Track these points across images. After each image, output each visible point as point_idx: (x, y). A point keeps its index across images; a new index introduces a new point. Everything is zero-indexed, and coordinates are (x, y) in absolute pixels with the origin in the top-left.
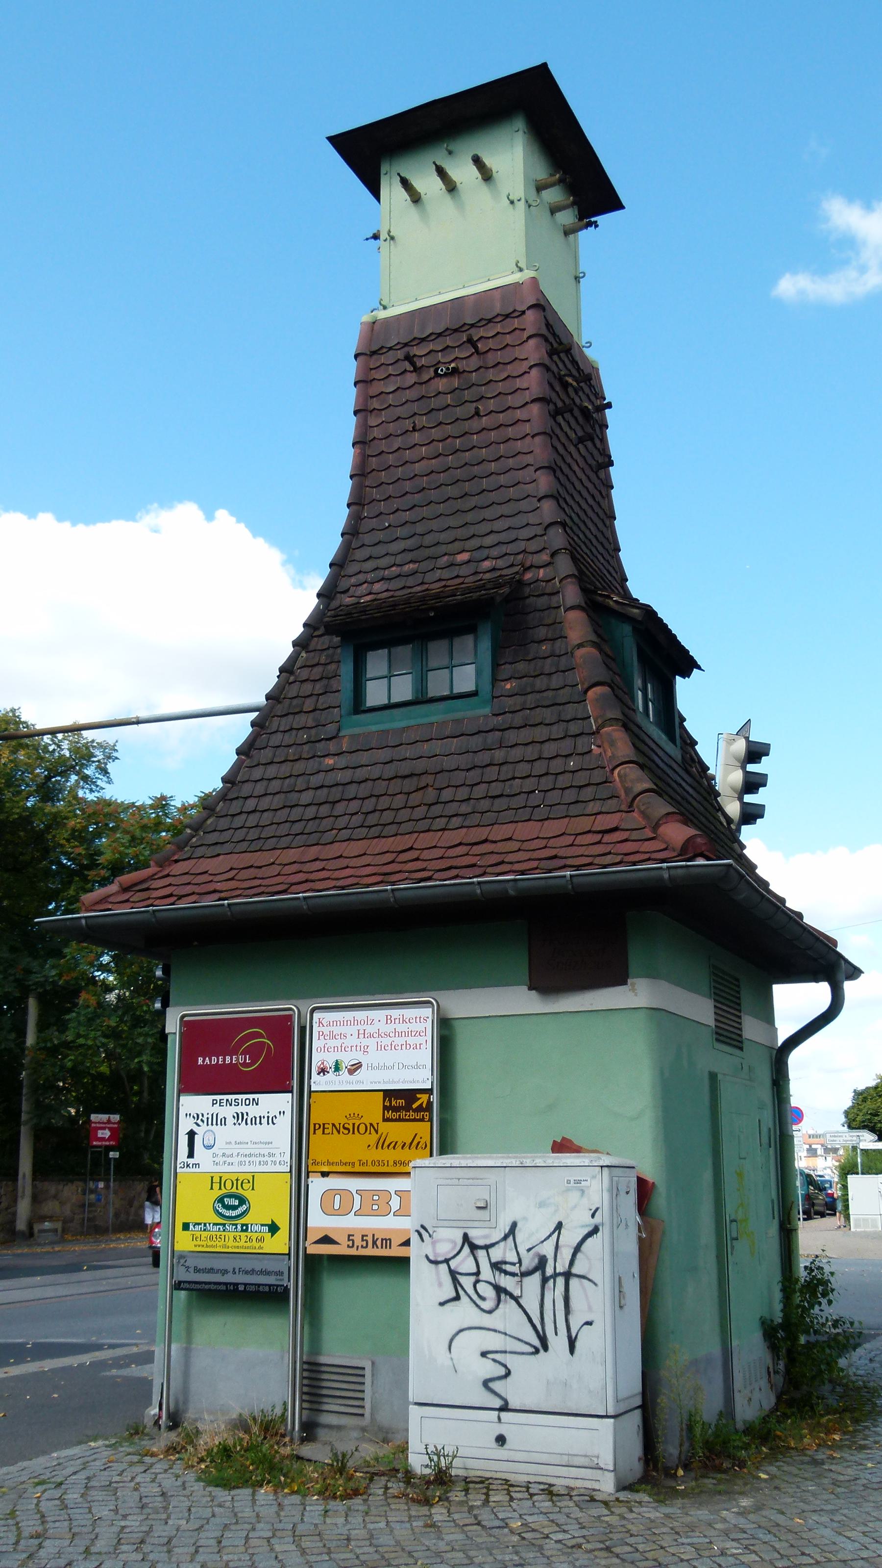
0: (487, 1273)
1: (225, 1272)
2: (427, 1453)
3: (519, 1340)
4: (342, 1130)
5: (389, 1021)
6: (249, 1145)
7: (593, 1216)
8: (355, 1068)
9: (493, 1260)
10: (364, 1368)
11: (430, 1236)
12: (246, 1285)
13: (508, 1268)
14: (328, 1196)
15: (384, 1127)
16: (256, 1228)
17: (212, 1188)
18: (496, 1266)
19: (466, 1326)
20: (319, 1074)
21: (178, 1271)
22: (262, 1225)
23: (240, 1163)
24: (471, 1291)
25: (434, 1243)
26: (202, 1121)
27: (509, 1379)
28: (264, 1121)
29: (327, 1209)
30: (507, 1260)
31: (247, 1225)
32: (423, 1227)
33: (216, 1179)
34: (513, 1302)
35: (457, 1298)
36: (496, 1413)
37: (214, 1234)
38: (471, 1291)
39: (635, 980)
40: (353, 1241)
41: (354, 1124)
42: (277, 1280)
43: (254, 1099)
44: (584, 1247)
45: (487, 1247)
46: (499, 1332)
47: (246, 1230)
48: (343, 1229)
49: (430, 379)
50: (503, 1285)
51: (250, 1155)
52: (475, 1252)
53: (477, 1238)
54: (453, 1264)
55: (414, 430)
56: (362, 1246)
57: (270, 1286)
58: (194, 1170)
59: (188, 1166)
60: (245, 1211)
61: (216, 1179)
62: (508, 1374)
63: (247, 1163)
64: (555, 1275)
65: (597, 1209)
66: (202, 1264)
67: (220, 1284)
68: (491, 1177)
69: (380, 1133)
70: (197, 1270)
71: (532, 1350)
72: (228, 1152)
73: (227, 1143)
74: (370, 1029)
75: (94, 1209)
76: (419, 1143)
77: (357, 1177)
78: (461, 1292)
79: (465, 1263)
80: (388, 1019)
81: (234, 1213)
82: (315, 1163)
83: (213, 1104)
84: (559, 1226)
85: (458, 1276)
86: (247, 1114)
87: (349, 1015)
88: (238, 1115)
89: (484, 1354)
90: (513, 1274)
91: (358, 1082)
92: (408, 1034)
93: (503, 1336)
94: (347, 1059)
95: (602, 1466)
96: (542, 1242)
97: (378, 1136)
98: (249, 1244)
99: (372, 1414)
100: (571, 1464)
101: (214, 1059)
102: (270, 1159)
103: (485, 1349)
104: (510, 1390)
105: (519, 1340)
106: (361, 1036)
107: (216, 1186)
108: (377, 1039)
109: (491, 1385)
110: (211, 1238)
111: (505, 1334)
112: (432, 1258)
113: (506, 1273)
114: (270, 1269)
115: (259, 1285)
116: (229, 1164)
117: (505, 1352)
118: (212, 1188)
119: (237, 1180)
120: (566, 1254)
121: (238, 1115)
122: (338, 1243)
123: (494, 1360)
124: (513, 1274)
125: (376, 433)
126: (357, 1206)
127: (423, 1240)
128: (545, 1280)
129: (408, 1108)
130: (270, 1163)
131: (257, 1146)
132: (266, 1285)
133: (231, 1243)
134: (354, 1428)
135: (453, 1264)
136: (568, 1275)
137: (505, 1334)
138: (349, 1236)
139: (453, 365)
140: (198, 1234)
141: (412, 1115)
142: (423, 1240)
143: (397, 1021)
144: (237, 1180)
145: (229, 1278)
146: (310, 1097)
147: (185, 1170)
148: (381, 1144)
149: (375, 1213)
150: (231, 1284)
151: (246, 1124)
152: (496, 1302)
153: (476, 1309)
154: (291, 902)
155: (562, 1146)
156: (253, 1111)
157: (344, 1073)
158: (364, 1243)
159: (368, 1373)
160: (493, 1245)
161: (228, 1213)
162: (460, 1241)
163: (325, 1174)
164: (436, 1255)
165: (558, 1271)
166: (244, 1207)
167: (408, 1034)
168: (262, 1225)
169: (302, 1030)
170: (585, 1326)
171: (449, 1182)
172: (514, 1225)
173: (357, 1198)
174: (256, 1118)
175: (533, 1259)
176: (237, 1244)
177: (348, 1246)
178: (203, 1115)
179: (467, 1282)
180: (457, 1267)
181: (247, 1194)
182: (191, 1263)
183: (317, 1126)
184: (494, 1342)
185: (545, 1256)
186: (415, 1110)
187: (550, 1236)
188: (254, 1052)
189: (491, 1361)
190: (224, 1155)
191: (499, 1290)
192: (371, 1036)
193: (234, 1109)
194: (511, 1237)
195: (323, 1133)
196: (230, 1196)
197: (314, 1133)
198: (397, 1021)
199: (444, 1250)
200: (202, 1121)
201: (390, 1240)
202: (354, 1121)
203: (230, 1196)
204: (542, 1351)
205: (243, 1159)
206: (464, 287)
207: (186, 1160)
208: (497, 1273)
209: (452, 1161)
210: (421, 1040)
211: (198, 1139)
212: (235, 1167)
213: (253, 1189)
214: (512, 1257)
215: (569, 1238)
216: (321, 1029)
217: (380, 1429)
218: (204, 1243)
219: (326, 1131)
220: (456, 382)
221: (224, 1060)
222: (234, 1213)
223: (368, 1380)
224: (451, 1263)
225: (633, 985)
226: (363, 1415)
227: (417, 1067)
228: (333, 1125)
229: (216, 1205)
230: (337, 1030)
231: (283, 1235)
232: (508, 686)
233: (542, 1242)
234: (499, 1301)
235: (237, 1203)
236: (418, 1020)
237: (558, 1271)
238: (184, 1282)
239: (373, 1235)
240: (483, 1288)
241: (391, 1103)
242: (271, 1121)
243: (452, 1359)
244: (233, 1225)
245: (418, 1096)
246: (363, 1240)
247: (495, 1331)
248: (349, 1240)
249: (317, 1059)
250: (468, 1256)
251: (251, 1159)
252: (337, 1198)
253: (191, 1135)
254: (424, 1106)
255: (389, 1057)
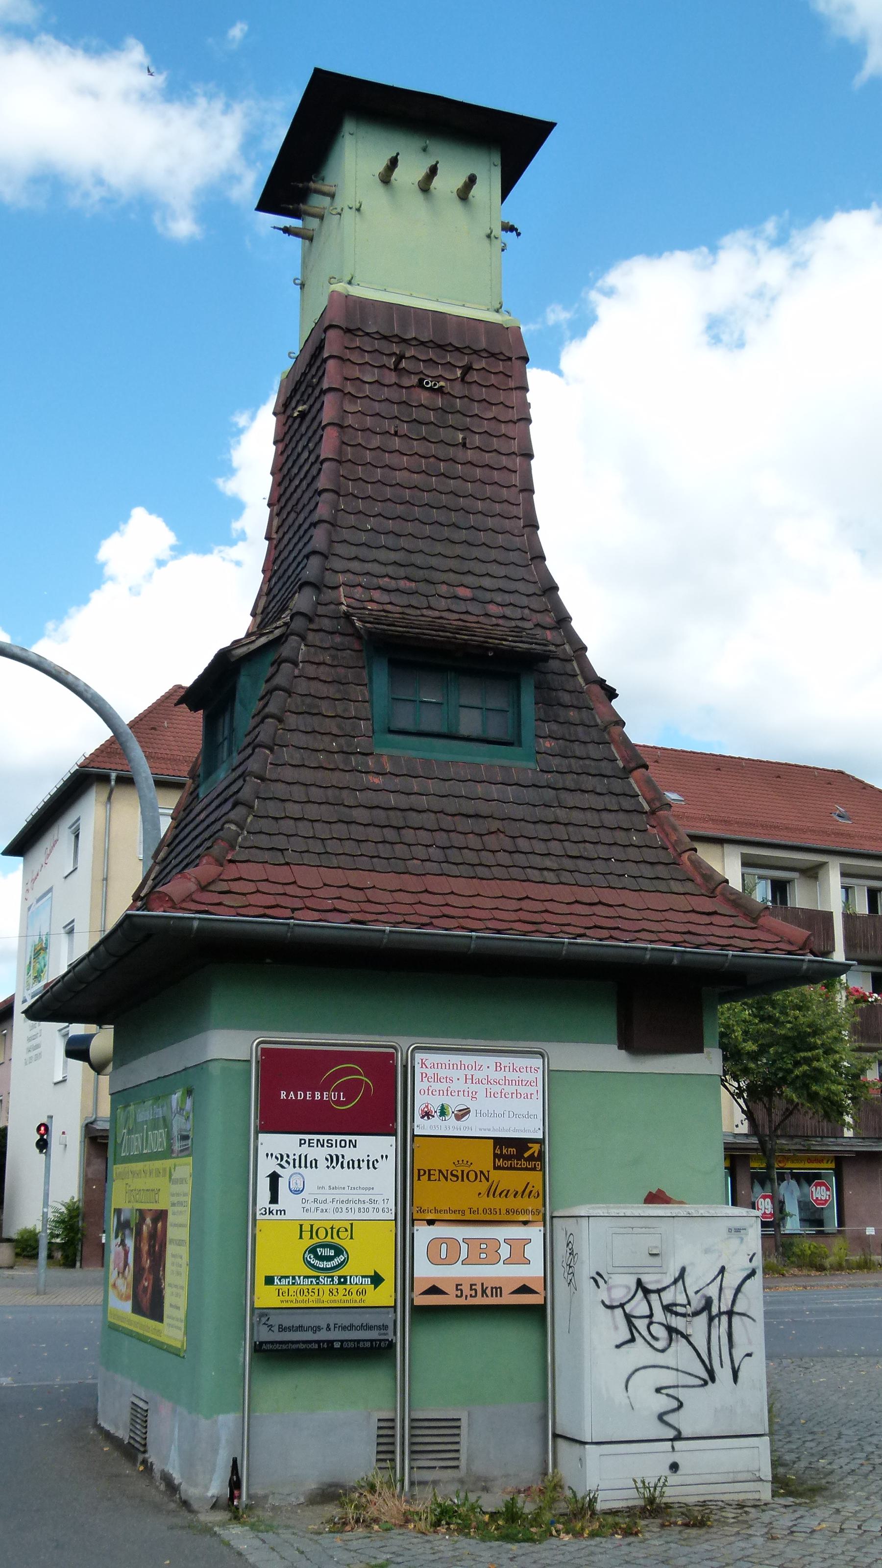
0: (659, 1315)
1: (316, 1329)
2: (637, 1488)
3: (690, 1374)
4: (450, 1176)
5: (499, 1069)
6: (347, 1191)
7: (751, 1260)
8: (462, 1114)
9: (665, 1303)
10: (459, 1420)
11: (606, 1282)
12: (342, 1341)
13: (680, 1309)
14: (434, 1245)
15: (495, 1175)
16: (356, 1280)
17: (301, 1237)
18: (668, 1308)
19: (641, 1365)
20: (423, 1117)
21: (258, 1332)
22: (363, 1277)
23: (336, 1210)
24: (645, 1333)
25: (609, 1289)
26: (288, 1163)
27: (682, 1411)
28: (364, 1165)
29: (434, 1258)
30: (678, 1302)
31: (345, 1277)
32: (598, 1274)
33: (307, 1227)
34: (684, 1341)
35: (633, 1340)
36: (670, 1443)
37: (305, 1287)
38: (645, 1333)
39: (709, 1049)
40: (461, 1290)
41: (463, 1172)
42: (380, 1334)
43: (350, 1141)
44: (744, 1288)
45: (659, 1291)
46: (672, 1369)
47: (345, 1283)
48: (453, 1279)
49: (412, 386)
50: (674, 1325)
51: (348, 1201)
52: (648, 1296)
53: (651, 1282)
54: (628, 1308)
55: (396, 434)
56: (471, 1296)
57: (371, 1341)
58: (279, 1217)
59: (271, 1212)
60: (342, 1262)
61: (307, 1227)
62: (681, 1405)
63: (344, 1210)
64: (720, 1314)
65: (754, 1254)
66: (288, 1321)
67: (310, 1342)
68: (664, 1227)
69: (490, 1181)
70: (282, 1329)
71: (702, 1382)
72: (321, 1198)
73: (319, 1188)
74: (478, 1075)
75: (844, 1264)
76: (531, 1192)
77: (468, 1225)
78: (636, 1334)
79: (639, 1307)
80: (498, 1067)
81: (329, 1265)
82: (421, 1211)
83: (301, 1144)
84: (722, 1270)
85: (633, 1319)
86: (343, 1156)
87: (455, 1058)
88: (331, 1157)
89: (658, 1390)
90: (684, 1315)
91: (466, 1128)
92: (520, 1082)
93: (675, 1372)
94: (454, 1104)
95: (763, 1478)
96: (708, 1285)
97: (489, 1184)
98: (348, 1298)
99: (468, 1465)
100: (736, 1479)
101: (300, 1095)
102: (371, 1206)
103: (659, 1386)
104: (681, 1420)
105: (690, 1374)
106: (469, 1081)
107: (307, 1235)
108: (486, 1086)
109: (666, 1418)
110: (302, 1292)
111: (677, 1370)
112: (607, 1303)
113: (677, 1314)
114: (372, 1323)
115: (359, 1341)
116: (322, 1211)
117: (677, 1386)
118: (301, 1237)
119: (332, 1228)
120: (728, 1295)
121: (331, 1157)
122: (446, 1294)
123: (668, 1395)
124: (684, 1315)
125: (350, 420)
126: (464, 1255)
127: (598, 1287)
128: (711, 1319)
129: (519, 1156)
130: (371, 1210)
131: (355, 1191)
132: (367, 1341)
133: (326, 1297)
134: (453, 1480)
135: (628, 1308)
136: (730, 1313)
137: (677, 1370)
138: (457, 1285)
139: (442, 383)
140: (285, 1288)
141: (524, 1164)
142: (598, 1287)
143: (507, 1069)
144: (332, 1228)
145: (323, 1335)
146: (413, 1141)
147: (267, 1217)
148: (491, 1192)
149: (485, 1261)
150: (324, 1342)
151: (342, 1167)
152: (668, 1341)
153: (650, 1349)
154: (508, 942)
155: (656, 1198)
156: (349, 1154)
157: (451, 1120)
158: (473, 1293)
159: (464, 1424)
160: (664, 1289)
161: (321, 1265)
162: (633, 1287)
163: (431, 1222)
164: (611, 1300)
165: (722, 1310)
166: (342, 1258)
167: (520, 1082)
168: (363, 1277)
169: (405, 1067)
170: (747, 1358)
171: (622, 1231)
172: (683, 1270)
173: (464, 1247)
174: (353, 1161)
175: (700, 1301)
176: (333, 1298)
177: (457, 1296)
178: (288, 1156)
179: (641, 1324)
180: (632, 1310)
181: (345, 1243)
182: (275, 1320)
183: (422, 1172)
184: (666, 1378)
185: (711, 1297)
186: (526, 1160)
187: (715, 1279)
188: (350, 1089)
189: (665, 1396)
190: (315, 1201)
191: (671, 1330)
192: (480, 1082)
193: (326, 1151)
194: (681, 1282)
195: (429, 1179)
196: (323, 1246)
197: (419, 1179)
198: (507, 1069)
199: (619, 1295)
200: (288, 1163)
201: (500, 1288)
202: (462, 1168)
203: (323, 1246)
204: (710, 1383)
205: (339, 1205)
206: (437, 301)
207: (268, 1206)
208: (669, 1315)
209: (624, 1211)
210: (533, 1090)
211: (282, 1184)
212: (331, 1214)
213: (352, 1238)
214: (682, 1299)
215: (732, 1280)
216: (424, 1070)
217: (478, 1479)
218: (293, 1298)
219: (432, 1178)
220: (439, 401)
221: (313, 1096)
222: (329, 1265)
223: (464, 1431)
224: (625, 1307)
225: (709, 1053)
226: (457, 1467)
227: (529, 1116)
228: (440, 1171)
229: (307, 1256)
230: (442, 1073)
231: (387, 1286)
232: (548, 744)
233: (708, 1285)
234: (671, 1340)
235: (332, 1253)
236: (529, 1069)
237: (722, 1310)
238: (266, 1343)
239: (482, 1284)
240: (654, 1328)
241: (501, 1151)
242: (372, 1165)
243: (628, 1397)
244: (328, 1277)
245: (530, 1145)
246: (471, 1289)
247: (668, 1368)
248: (457, 1290)
249: (420, 1102)
250: (641, 1300)
251: (349, 1206)
252: (444, 1246)
253: (274, 1178)
254: (536, 1155)
255: (498, 1105)
